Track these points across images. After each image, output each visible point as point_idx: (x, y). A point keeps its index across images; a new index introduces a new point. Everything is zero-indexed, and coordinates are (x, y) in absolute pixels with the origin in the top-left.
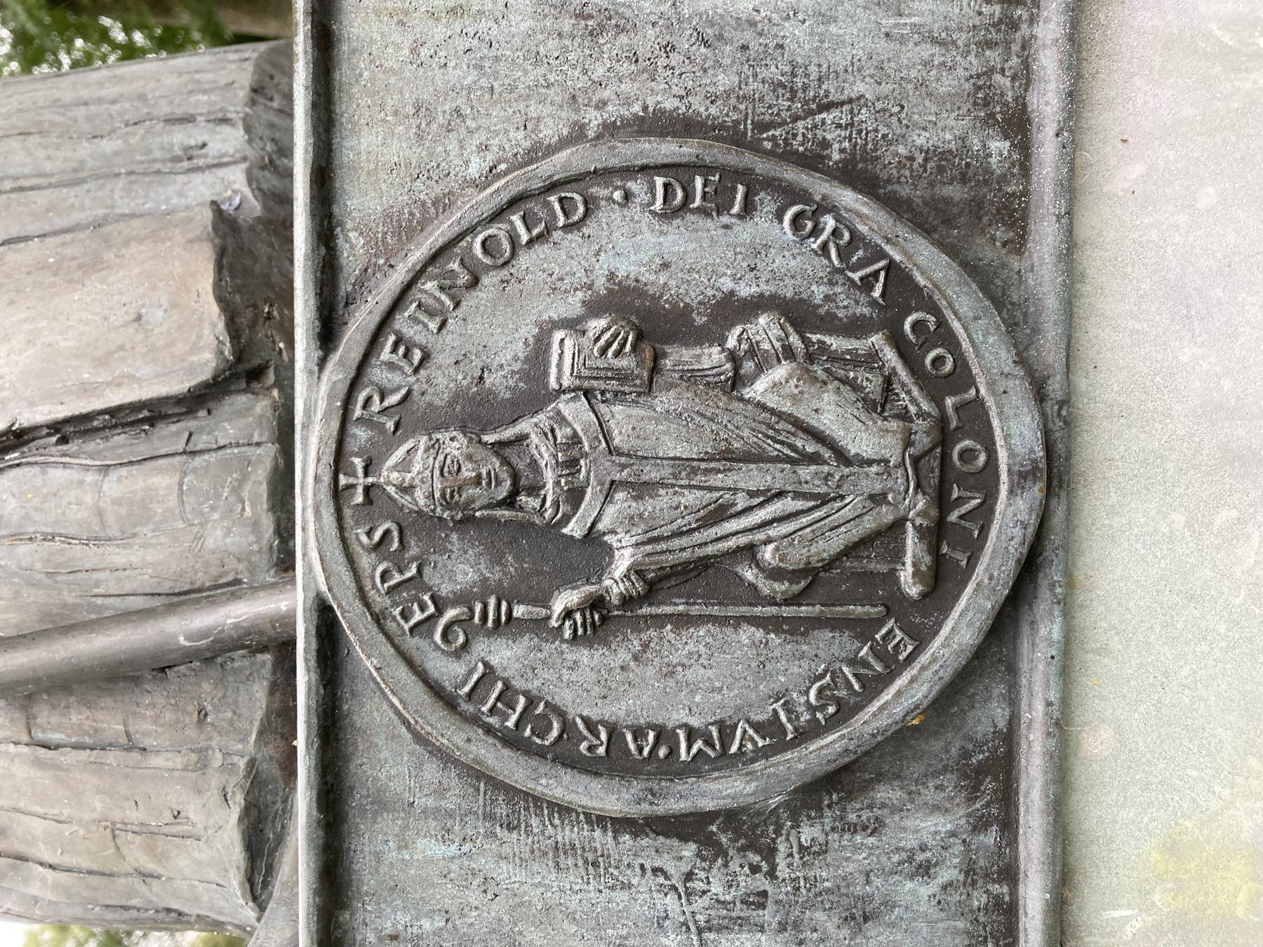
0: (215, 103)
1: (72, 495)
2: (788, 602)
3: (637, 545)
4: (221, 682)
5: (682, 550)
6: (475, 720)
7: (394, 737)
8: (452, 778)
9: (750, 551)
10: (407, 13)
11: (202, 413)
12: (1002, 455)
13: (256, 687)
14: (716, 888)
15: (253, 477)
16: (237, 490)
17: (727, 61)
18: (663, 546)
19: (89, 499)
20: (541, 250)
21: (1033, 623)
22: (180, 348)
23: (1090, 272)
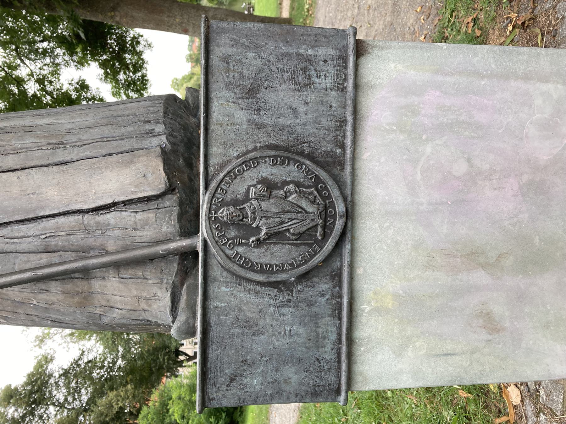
0: (155, 117)
1: (128, 218)
2: (295, 240)
3: (266, 229)
4: (166, 263)
5: (275, 230)
6: (235, 262)
7: (217, 267)
8: (229, 275)
9: (288, 230)
10: (222, 124)
11: (160, 199)
12: (337, 212)
13: (175, 264)
14: (281, 298)
15: (174, 214)
16: (170, 218)
17: (285, 134)
18: (271, 229)
19: (133, 219)
20: (248, 171)
21: (345, 245)
22: (156, 183)
23: (359, 175)
